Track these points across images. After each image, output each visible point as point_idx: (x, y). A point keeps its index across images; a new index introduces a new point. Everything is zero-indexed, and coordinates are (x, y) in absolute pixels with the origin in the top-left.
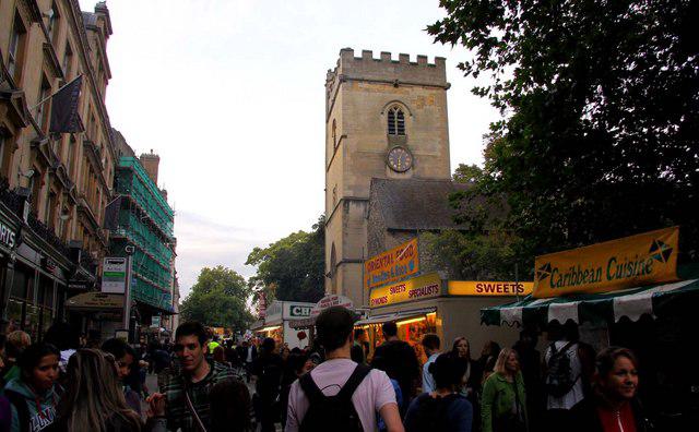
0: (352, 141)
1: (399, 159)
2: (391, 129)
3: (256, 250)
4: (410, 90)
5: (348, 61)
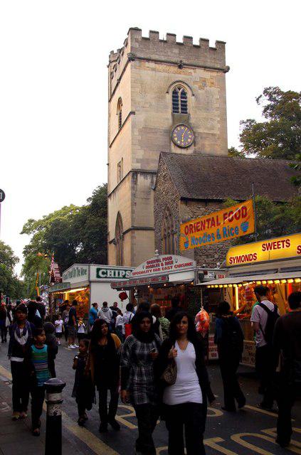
0: (140, 117)
1: (183, 136)
2: (175, 109)
3: (31, 221)
4: (192, 71)
5: (137, 41)
